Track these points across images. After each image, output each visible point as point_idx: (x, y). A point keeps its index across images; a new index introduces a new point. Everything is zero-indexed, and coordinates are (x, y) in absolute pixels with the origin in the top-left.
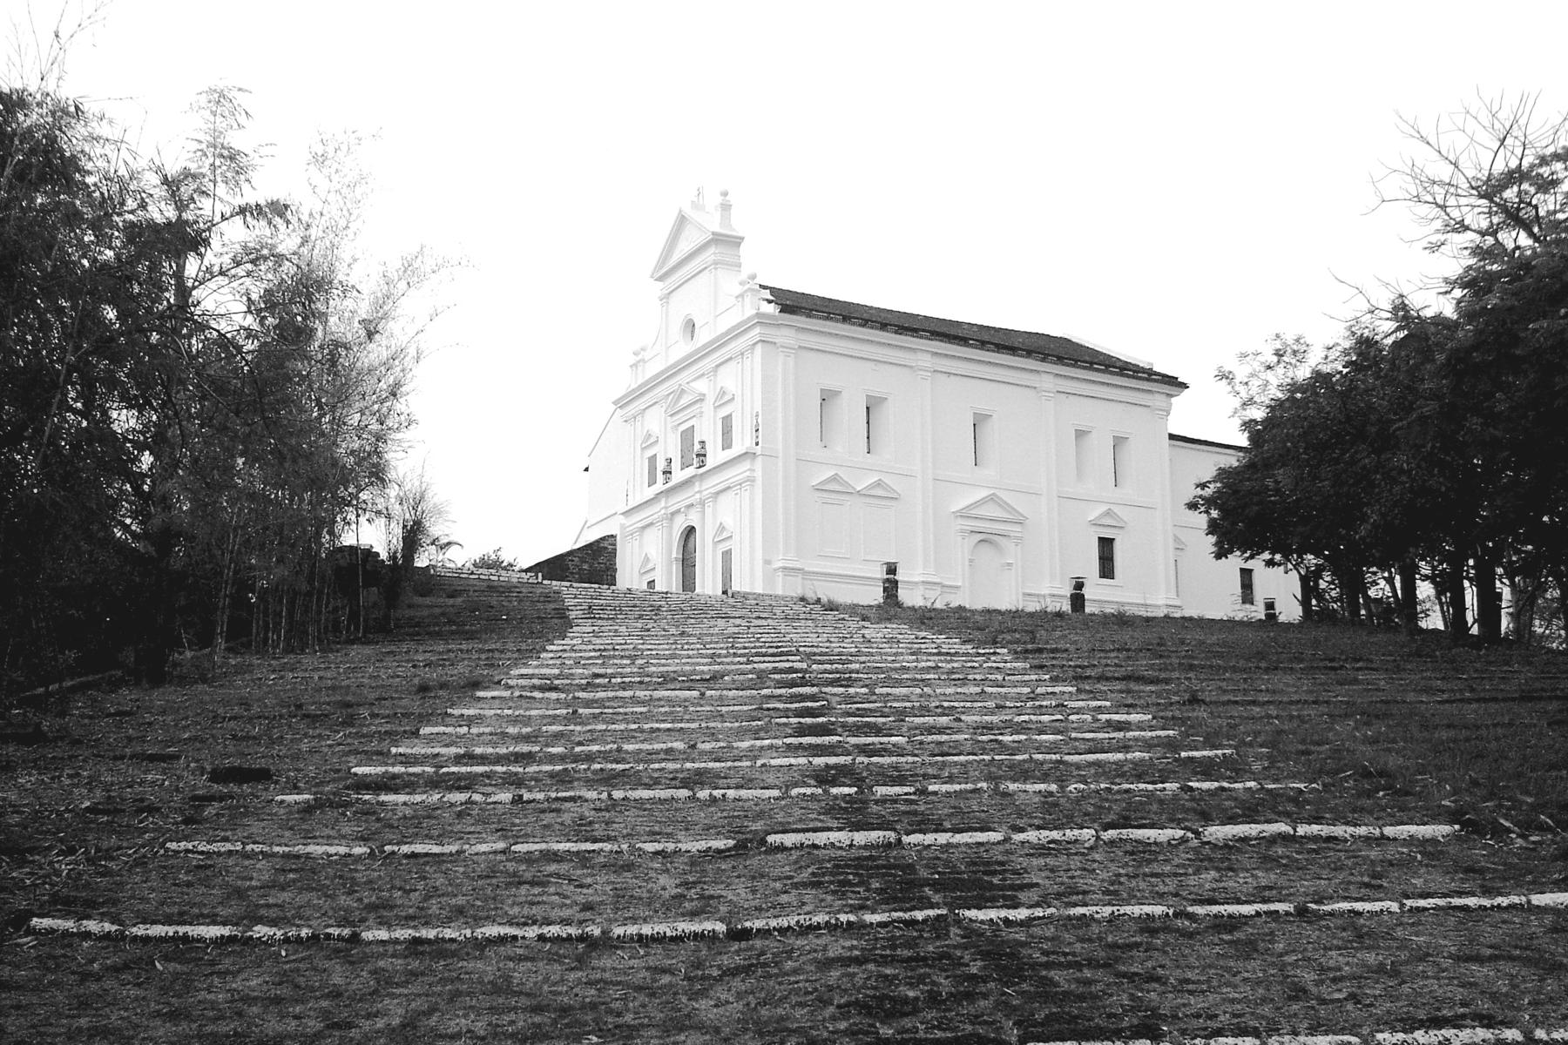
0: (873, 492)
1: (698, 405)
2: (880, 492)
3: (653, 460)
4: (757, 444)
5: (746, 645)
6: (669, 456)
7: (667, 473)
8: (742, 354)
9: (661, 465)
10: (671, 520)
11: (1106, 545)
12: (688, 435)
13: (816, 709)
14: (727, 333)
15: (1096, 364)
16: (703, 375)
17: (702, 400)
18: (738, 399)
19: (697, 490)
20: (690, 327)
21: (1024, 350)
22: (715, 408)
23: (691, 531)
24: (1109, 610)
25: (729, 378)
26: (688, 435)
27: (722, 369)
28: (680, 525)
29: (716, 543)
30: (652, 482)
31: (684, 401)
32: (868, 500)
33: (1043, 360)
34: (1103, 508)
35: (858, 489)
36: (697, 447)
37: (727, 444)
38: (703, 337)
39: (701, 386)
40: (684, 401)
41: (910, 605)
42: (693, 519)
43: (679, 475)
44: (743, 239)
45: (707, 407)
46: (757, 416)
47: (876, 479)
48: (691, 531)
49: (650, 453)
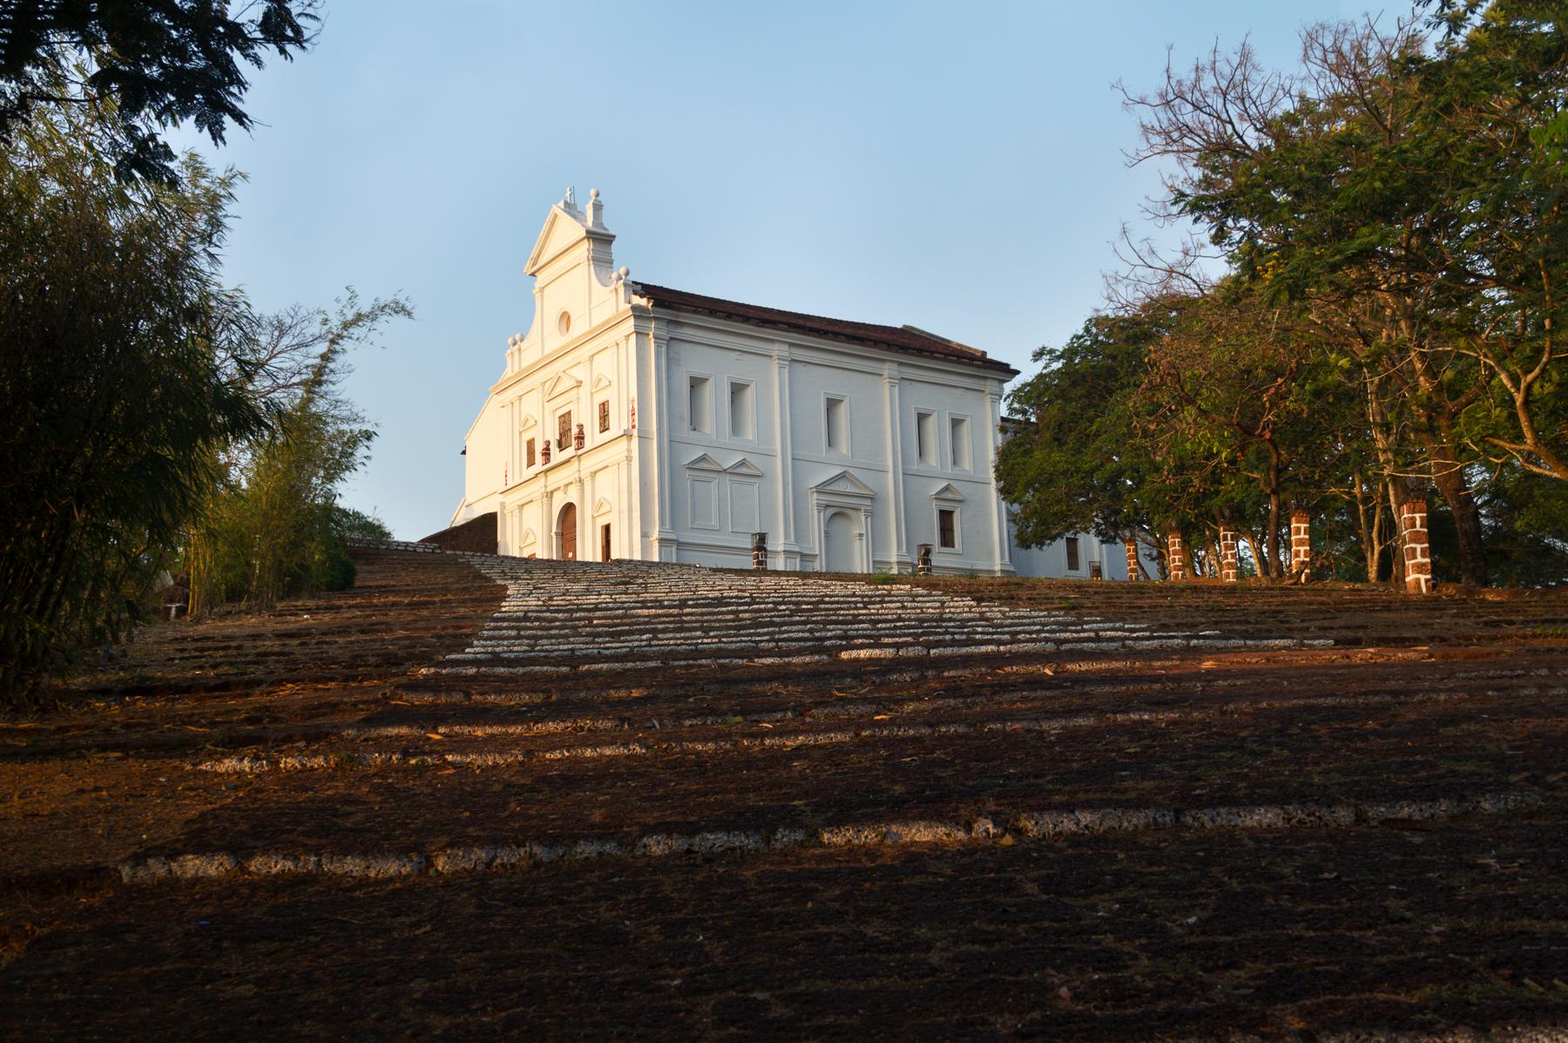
0: (738, 470)
1: (576, 390)
2: (744, 470)
3: (531, 443)
6: (547, 438)
7: (546, 453)
9: (539, 448)
11: (946, 517)
12: (565, 419)
18: (615, 384)
20: (565, 318)
22: (592, 394)
23: (569, 509)
25: (605, 365)
26: (565, 419)
28: (559, 503)
29: (594, 518)
30: (531, 462)
34: (944, 484)
36: (575, 431)
37: (604, 428)
38: (579, 328)
39: (579, 373)
42: (572, 496)
43: (557, 456)
44: (614, 237)
45: (584, 391)
47: (701, 454)
48: (569, 509)
49: (527, 437)
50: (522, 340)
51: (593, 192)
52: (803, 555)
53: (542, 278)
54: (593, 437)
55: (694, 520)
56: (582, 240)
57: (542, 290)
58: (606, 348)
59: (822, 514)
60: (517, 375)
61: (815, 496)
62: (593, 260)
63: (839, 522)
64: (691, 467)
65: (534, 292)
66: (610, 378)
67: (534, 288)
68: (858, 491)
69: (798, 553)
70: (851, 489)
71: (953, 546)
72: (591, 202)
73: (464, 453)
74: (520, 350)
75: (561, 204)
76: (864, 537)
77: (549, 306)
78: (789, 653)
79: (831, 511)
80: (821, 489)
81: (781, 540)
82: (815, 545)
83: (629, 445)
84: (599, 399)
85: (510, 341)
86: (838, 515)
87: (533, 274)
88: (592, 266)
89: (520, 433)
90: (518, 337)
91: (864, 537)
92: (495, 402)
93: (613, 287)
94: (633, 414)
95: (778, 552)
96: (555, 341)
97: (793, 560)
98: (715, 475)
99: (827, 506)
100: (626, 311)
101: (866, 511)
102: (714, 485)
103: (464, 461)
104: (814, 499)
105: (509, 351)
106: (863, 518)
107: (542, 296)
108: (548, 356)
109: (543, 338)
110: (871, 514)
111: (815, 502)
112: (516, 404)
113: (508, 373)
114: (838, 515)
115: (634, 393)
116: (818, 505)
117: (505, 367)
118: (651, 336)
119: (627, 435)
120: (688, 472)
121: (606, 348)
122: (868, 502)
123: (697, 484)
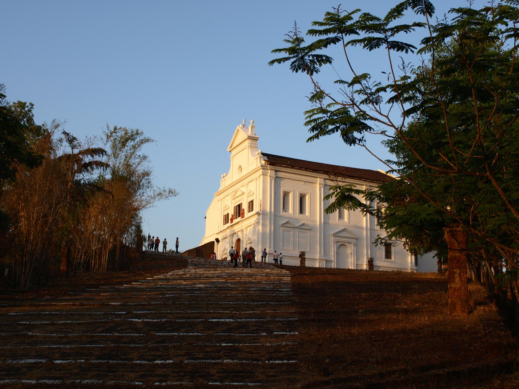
0: (302, 227)
2: (288, 225)
4: (261, 210)
5: (104, 259)
8: (256, 179)
10: (233, 236)
13: (202, 288)
14: (252, 171)
15: (295, 167)
16: (244, 185)
17: (243, 194)
18: (255, 194)
19: (241, 226)
21: (358, 177)
22: (248, 197)
24: (395, 270)
25: (252, 187)
27: (250, 184)
31: (238, 195)
32: (300, 230)
33: (365, 181)
35: (297, 226)
38: (245, 172)
39: (243, 189)
40: (238, 195)
41: (184, 251)
45: (245, 196)
46: (261, 200)
47: (287, 221)
50: (226, 176)
51: (251, 121)
52: (326, 261)
53: (233, 152)
54: (247, 214)
55: (283, 246)
56: (389, 51)
57: (233, 157)
58: (253, 180)
59: (335, 245)
60: (223, 189)
61: (333, 238)
62: (250, 147)
63: (342, 248)
64: (283, 225)
65: (230, 158)
66: (254, 192)
67: (230, 156)
68: (351, 236)
69: (324, 260)
70: (347, 235)
71: (391, 258)
72: (251, 125)
73: (205, 218)
74: (225, 179)
75: (240, 126)
76: (353, 254)
77: (236, 162)
78: (189, 318)
79: (339, 244)
80: (335, 235)
81: (318, 255)
82: (332, 256)
83: (259, 217)
84: (250, 199)
85: (222, 176)
86: (341, 245)
87: (230, 151)
88: (250, 149)
89: (224, 211)
90: (225, 174)
91: (353, 254)
92: (216, 199)
93: (256, 157)
94: (261, 206)
95: (316, 259)
96: (236, 177)
97: (322, 263)
98: (292, 229)
99: (338, 242)
100: (259, 167)
101: (353, 244)
102: (292, 233)
103: (206, 220)
104: (332, 239)
105: (221, 180)
106: (353, 247)
107: (233, 159)
108: (234, 182)
109: (233, 175)
110: (356, 245)
111: (333, 240)
112: (223, 200)
113: (221, 188)
114: (341, 245)
115: (261, 198)
116: (334, 241)
117: (220, 186)
118: (268, 176)
119: (258, 213)
120: (281, 227)
121: (253, 180)
122: (355, 240)
123: (285, 232)
